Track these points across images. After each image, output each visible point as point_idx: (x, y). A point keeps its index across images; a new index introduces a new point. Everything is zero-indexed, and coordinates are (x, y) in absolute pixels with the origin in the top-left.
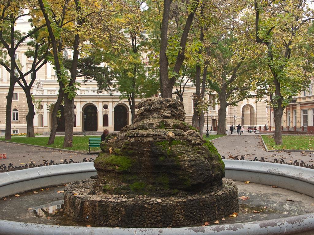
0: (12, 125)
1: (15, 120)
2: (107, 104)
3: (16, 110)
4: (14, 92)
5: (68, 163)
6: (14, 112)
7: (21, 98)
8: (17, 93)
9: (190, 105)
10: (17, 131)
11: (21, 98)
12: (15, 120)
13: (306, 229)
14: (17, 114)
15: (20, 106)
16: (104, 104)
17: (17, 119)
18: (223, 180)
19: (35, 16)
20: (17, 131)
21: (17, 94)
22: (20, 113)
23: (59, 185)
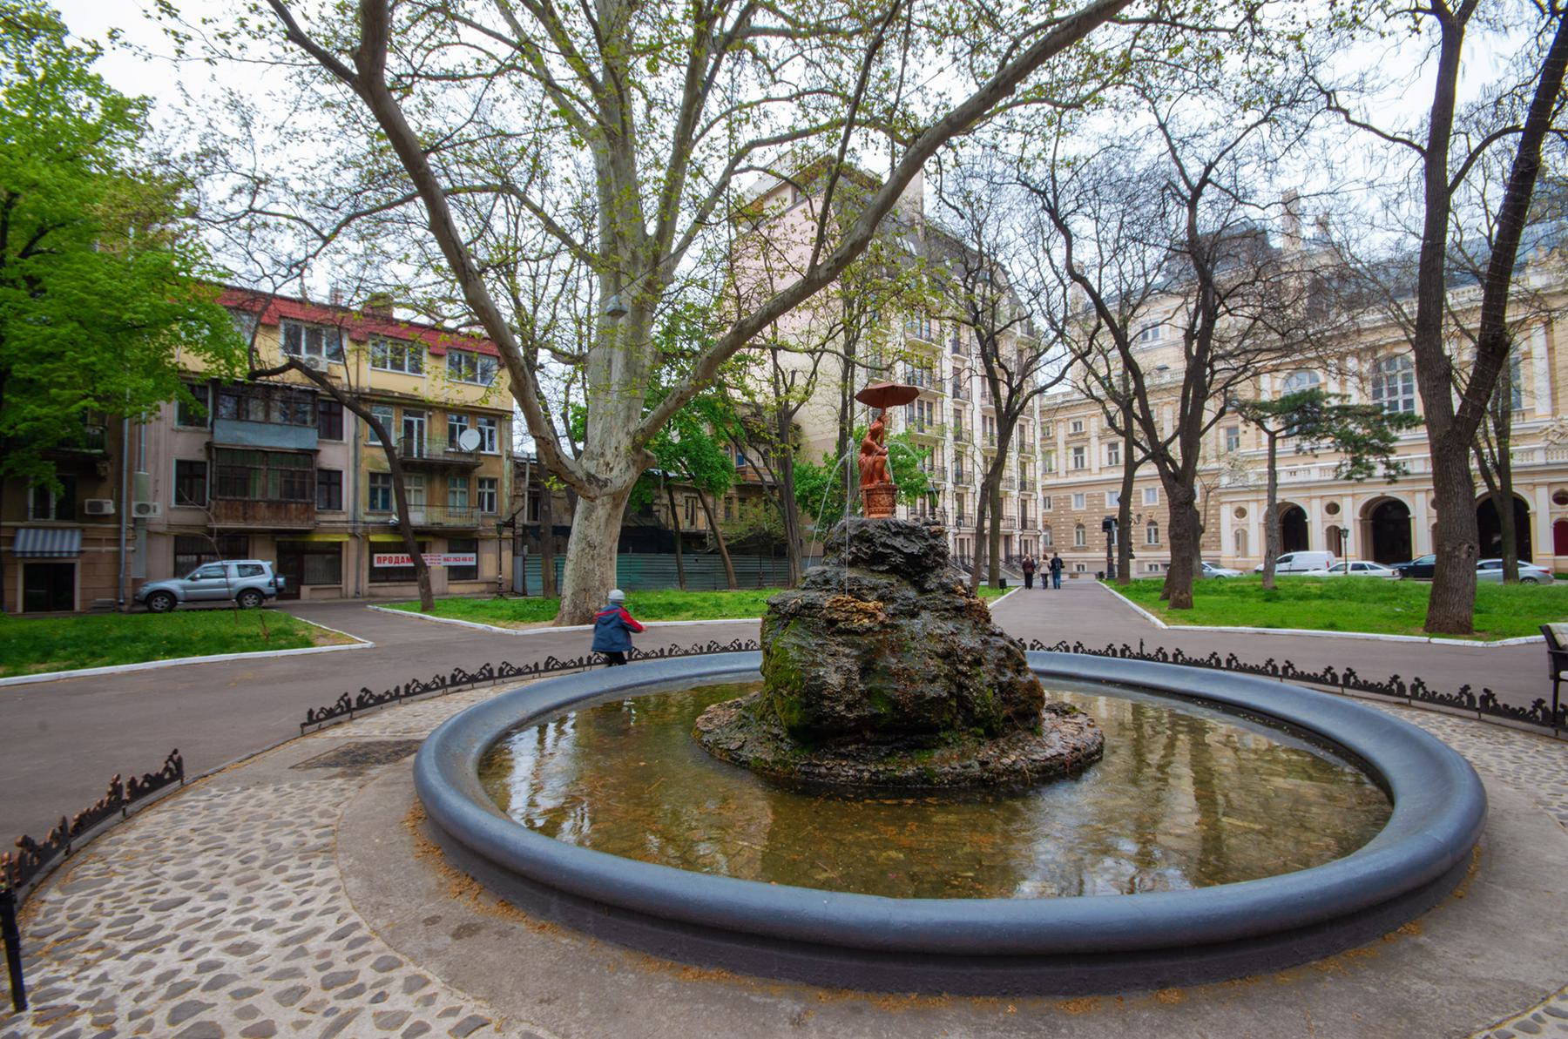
2: (1243, 505)
16: (1236, 506)
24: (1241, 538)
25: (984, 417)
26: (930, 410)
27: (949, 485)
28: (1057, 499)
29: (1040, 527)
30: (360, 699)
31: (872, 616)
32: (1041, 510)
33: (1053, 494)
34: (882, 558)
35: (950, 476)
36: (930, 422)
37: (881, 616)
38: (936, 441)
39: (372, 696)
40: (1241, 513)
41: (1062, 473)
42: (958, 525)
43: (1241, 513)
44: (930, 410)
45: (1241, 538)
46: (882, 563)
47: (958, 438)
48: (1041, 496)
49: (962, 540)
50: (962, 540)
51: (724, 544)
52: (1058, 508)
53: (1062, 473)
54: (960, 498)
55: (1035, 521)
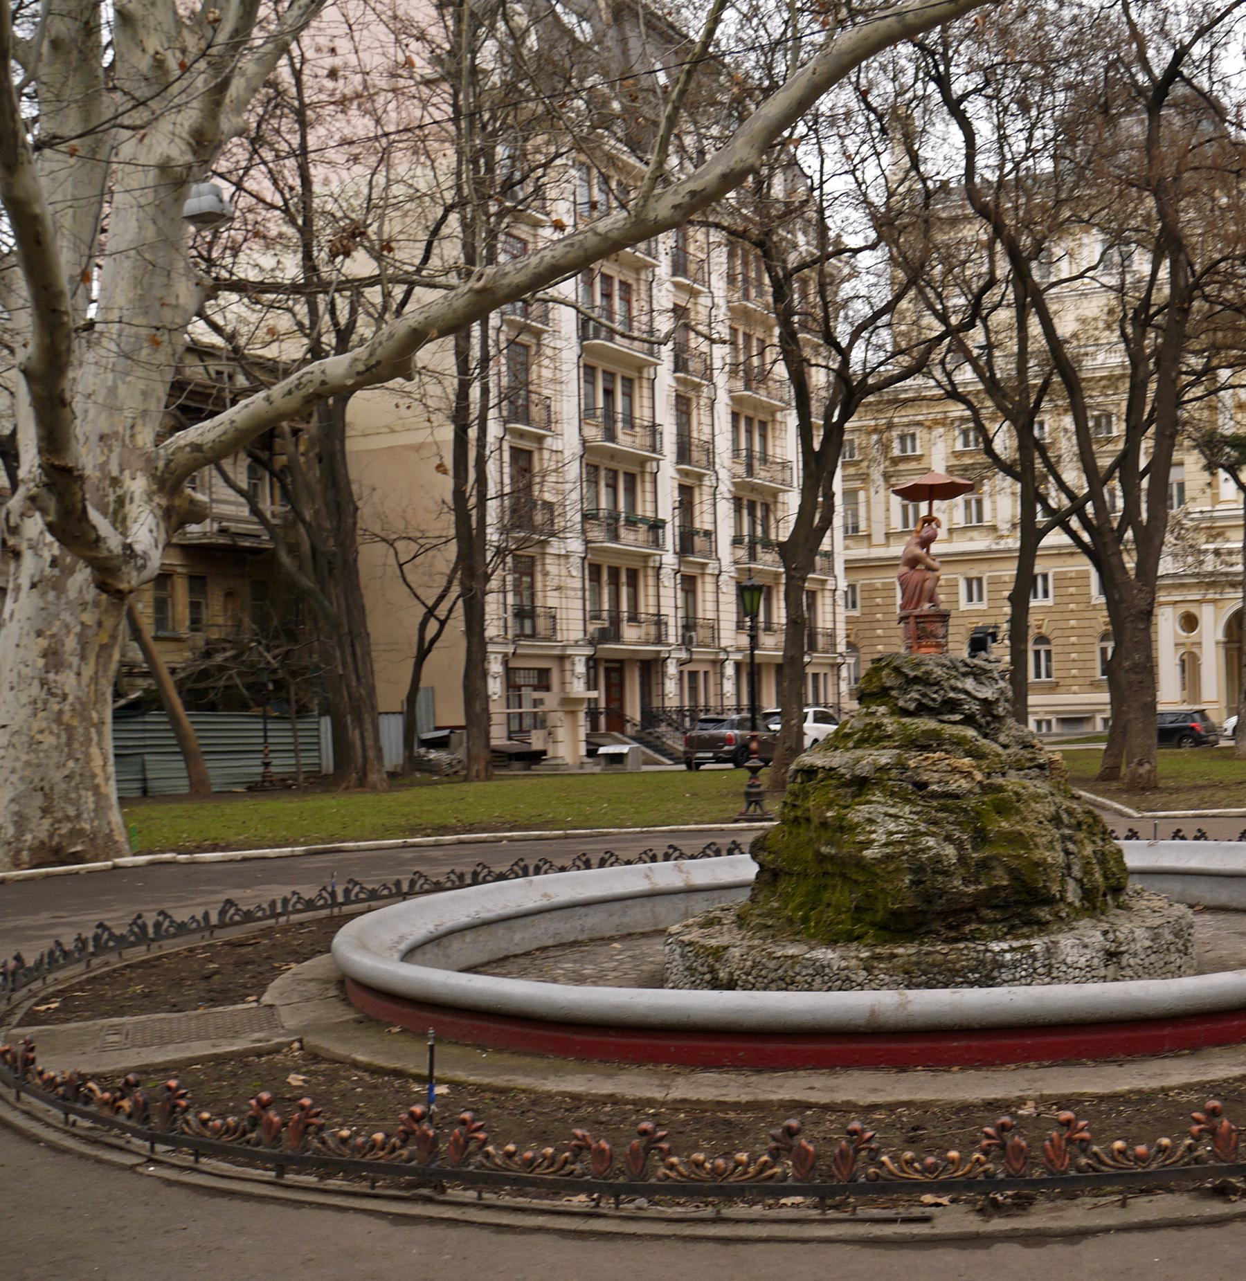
0: (1032, 699)
1: (1044, 678)
2: (1193, 609)
3: (1042, 639)
4: (1038, 569)
5: (595, 861)
6: (1037, 647)
7: (1063, 591)
8: (980, 580)
9: (1089, 664)
10: (548, 671)
11: (1063, 591)
12: (1044, 678)
13: (376, 496)
14: (1048, 653)
15: (1061, 624)
16: (1182, 609)
17: (1049, 675)
18: (900, 47)
19: (1159, 319)
20: (548, 671)
21: (1045, 577)
22: (1059, 649)
23: (560, 946)
24: (1189, 665)
25: (735, 416)
26: (628, 395)
27: (669, 559)
28: (871, 589)
29: (841, 648)
30: (97, 938)
31: (968, 775)
32: (842, 613)
33: (862, 579)
34: (952, 706)
35: (670, 536)
36: (630, 421)
37: (979, 776)
38: (643, 461)
39: (112, 935)
40: (1190, 622)
41: (878, 538)
42: (686, 642)
43: (1190, 622)
44: (628, 395)
45: (1189, 665)
46: (952, 712)
47: (684, 453)
48: (842, 584)
49: (693, 675)
50: (693, 675)
51: (169, 683)
52: (871, 608)
53: (878, 538)
54: (689, 585)
55: (832, 635)
